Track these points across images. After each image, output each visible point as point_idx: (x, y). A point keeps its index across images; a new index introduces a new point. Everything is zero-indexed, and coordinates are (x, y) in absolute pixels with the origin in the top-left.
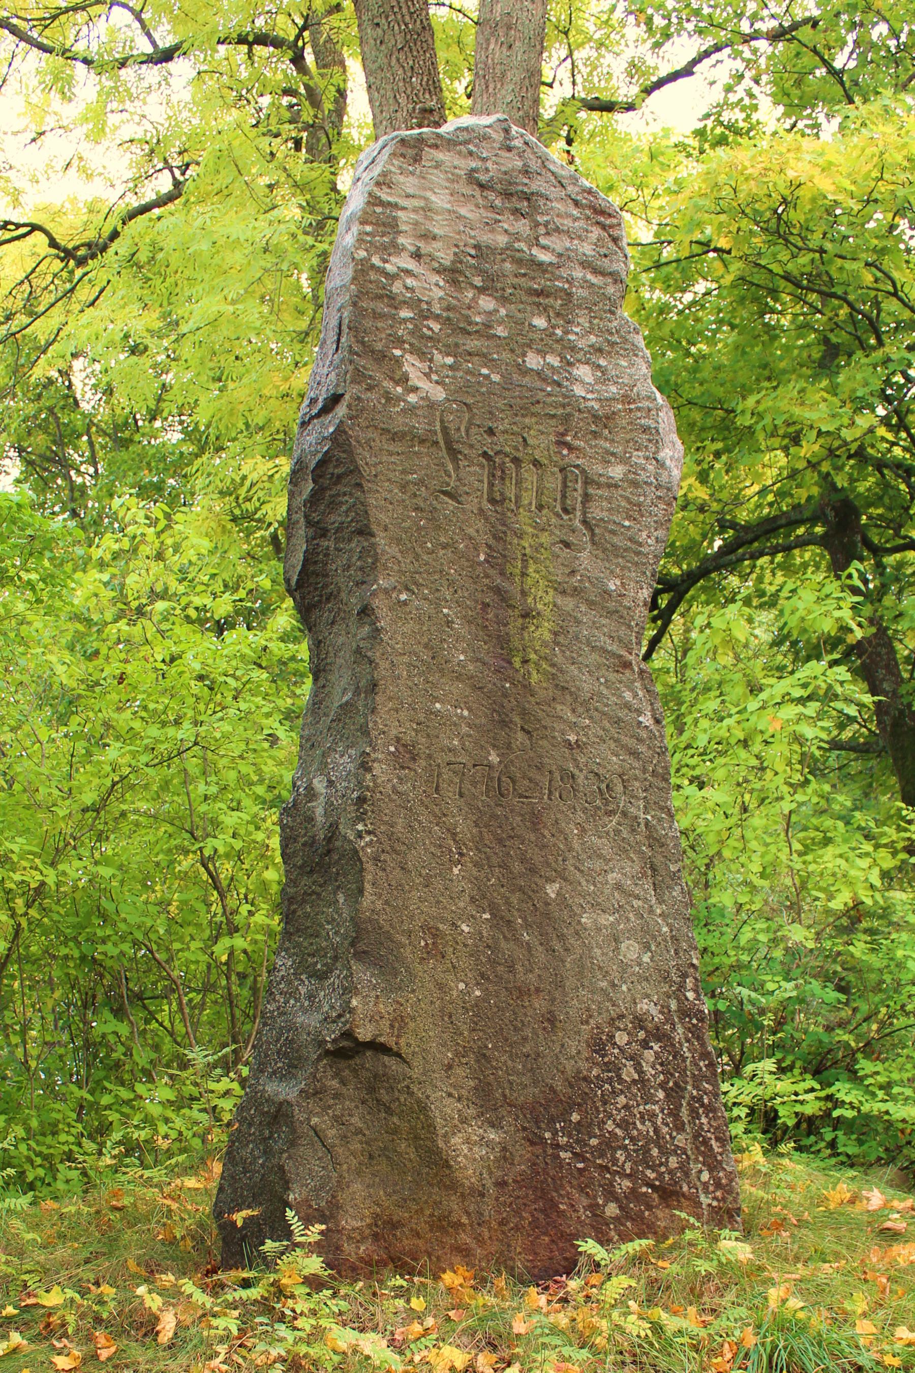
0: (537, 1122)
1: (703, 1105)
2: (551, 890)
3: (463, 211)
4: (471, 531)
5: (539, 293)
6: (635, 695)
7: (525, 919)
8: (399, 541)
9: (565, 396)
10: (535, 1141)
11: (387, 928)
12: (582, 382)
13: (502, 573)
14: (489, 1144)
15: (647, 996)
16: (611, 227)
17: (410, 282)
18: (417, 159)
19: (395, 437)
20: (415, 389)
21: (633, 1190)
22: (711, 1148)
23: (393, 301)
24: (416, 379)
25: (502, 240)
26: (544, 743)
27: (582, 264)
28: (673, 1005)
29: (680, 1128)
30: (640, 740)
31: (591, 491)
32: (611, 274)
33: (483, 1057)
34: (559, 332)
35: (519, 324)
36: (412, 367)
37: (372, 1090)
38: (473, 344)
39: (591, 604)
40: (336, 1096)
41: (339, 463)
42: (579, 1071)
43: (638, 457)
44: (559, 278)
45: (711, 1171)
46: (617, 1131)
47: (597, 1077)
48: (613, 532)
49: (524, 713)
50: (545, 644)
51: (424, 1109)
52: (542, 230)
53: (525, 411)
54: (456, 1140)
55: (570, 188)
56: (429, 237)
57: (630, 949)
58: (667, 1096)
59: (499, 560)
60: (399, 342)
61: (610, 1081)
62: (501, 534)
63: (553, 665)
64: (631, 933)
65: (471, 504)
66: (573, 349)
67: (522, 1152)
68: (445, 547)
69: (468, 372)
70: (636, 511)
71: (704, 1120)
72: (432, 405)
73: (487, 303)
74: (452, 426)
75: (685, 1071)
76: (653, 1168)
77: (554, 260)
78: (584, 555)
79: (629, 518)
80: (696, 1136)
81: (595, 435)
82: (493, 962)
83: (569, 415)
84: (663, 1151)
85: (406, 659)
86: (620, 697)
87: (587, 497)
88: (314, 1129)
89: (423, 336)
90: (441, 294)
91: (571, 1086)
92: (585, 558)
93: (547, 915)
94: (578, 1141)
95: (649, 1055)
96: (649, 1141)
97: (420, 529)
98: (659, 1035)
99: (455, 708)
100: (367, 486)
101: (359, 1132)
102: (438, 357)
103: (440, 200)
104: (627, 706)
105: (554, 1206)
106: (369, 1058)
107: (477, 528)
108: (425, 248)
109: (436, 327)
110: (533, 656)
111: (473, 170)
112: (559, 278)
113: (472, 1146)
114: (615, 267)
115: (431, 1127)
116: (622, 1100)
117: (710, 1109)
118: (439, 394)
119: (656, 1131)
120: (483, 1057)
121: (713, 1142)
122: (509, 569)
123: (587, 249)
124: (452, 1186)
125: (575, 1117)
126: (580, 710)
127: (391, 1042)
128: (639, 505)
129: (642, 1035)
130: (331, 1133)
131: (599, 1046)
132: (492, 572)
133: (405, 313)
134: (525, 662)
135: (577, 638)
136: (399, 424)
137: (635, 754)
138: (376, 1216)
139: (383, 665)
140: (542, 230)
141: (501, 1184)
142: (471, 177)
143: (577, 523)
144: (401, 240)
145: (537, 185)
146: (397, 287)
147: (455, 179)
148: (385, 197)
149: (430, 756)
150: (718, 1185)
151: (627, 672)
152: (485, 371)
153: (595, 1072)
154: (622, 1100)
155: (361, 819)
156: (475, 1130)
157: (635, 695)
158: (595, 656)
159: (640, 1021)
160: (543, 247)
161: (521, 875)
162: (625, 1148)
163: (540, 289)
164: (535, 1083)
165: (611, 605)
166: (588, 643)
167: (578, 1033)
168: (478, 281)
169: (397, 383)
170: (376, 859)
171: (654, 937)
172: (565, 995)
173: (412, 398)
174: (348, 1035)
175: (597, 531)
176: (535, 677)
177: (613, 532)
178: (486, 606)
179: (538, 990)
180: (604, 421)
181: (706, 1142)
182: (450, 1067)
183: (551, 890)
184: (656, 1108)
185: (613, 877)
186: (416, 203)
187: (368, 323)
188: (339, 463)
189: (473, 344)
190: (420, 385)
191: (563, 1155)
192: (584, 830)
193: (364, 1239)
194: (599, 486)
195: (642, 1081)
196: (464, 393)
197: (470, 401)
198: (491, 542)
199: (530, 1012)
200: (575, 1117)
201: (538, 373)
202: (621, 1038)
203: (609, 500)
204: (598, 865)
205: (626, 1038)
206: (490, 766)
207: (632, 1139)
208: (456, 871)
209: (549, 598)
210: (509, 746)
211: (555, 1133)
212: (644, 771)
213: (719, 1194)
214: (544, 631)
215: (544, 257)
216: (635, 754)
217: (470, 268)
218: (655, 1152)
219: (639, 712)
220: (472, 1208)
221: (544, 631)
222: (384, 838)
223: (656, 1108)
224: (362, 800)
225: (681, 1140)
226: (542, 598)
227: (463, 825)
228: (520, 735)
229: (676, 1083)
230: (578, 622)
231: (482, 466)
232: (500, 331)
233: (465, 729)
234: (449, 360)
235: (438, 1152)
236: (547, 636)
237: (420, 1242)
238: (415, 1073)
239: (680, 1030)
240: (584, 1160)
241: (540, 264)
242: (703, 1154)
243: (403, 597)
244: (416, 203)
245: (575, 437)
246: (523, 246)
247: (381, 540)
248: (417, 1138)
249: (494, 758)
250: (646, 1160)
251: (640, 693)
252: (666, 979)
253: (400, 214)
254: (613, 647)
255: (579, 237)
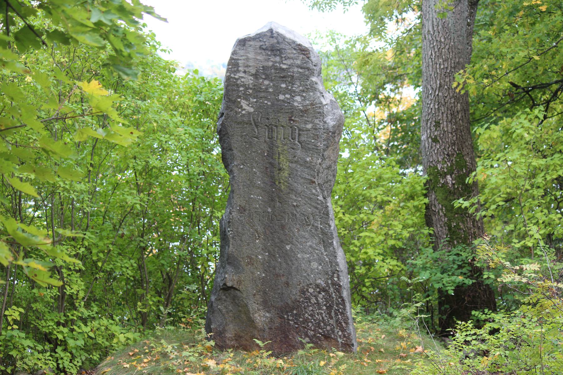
0: (282, 312)
1: (339, 312)
2: (288, 247)
3: (258, 58)
4: (262, 147)
5: (283, 77)
6: (316, 191)
7: (279, 255)
8: (240, 151)
9: (291, 106)
10: (282, 317)
11: (236, 256)
12: (297, 101)
13: (272, 158)
14: (266, 317)
15: (320, 279)
16: (307, 54)
17: (242, 80)
18: (244, 45)
19: (238, 123)
20: (244, 110)
21: (315, 335)
22: (342, 325)
23: (238, 86)
24: (245, 106)
25: (270, 64)
26: (286, 205)
27: (297, 67)
28: (330, 282)
29: (332, 318)
30: (318, 204)
31: (301, 132)
32: (307, 68)
33: (265, 293)
34: (290, 88)
35: (276, 87)
36: (244, 103)
37: (234, 300)
38: (262, 94)
39: (301, 165)
40: (225, 301)
41: (224, 131)
42: (296, 299)
43: (317, 121)
44: (290, 72)
45: (342, 331)
46: (309, 317)
47: (303, 301)
48: (308, 144)
49: (279, 197)
50: (286, 177)
51: (247, 306)
52: (284, 59)
53: (279, 112)
54: (256, 315)
55: (292, 45)
56: (248, 66)
57: (314, 265)
58: (327, 308)
59: (271, 155)
60: (240, 97)
61: (307, 302)
62: (272, 146)
63: (289, 183)
64: (315, 260)
65: (262, 140)
66: (294, 92)
67: (277, 321)
68: (254, 152)
69: (261, 103)
70: (316, 137)
71: (340, 316)
72: (249, 113)
73: (266, 82)
74: (256, 119)
75: (333, 301)
76: (321, 329)
77: (288, 67)
78: (299, 152)
79: (314, 139)
80: (337, 321)
81: (302, 116)
82: (269, 267)
83: (293, 111)
84: (325, 324)
85: (242, 184)
86: (311, 191)
87: (299, 135)
88: (219, 309)
89: (247, 94)
90: (252, 82)
91: (294, 303)
92: (299, 152)
93: (287, 254)
94: (296, 319)
95: (321, 296)
96: (320, 321)
97: (246, 148)
98: (324, 290)
99: (257, 197)
100: (230, 137)
101: (231, 311)
102: (251, 100)
103: (251, 55)
104: (314, 194)
105: (288, 337)
106: (232, 291)
107: (264, 146)
108: (247, 70)
109: (251, 91)
110: (282, 181)
111: (262, 45)
112: (290, 72)
113: (261, 317)
114: (308, 66)
115: (248, 311)
116: (311, 308)
117: (342, 313)
118: (252, 110)
119: (323, 318)
120: (265, 293)
121: (343, 323)
122: (274, 157)
123: (298, 62)
124: (255, 328)
125: (295, 312)
126: (298, 196)
127: (237, 287)
128: (317, 135)
129: (318, 290)
130: (224, 310)
131: (303, 292)
132: (269, 158)
133: (241, 89)
134: (280, 183)
135: (296, 175)
136: (240, 120)
137: (317, 208)
138: (236, 334)
139: (236, 185)
140: (284, 59)
141: (270, 329)
142: (261, 48)
143: (296, 142)
144: (240, 69)
145: (282, 46)
146: (239, 82)
147: (256, 49)
148: (235, 57)
149: (250, 210)
150: (344, 336)
151: (314, 184)
152: (266, 102)
153: (301, 300)
154: (311, 308)
155: (229, 227)
156: (262, 313)
157: (316, 191)
158: (302, 180)
159: (317, 286)
160: (284, 64)
161: (278, 243)
162: (312, 322)
163: (284, 76)
164: (282, 301)
165: (308, 165)
166: (300, 177)
167: (296, 288)
168: (263, 77)
169: (239, 108)
170: (233, 238)
171: (323, 262)
172: (292, 277)
173: (244, 112)
174: (225, 284)
175: (303, 144)
176: (283, 187)
177: (308, 144)
178: (267, 168)
179: (283, 275)
180: (305, 111)
181: (340, 323)
182: (254, 295)
183: (288, 247)
184: (323, 312)
185: (308, 244)
186: (244, 58)
187: (230, 93)
188: (224, 131)
189: (262, 94)
190: (246, 108)
191: (290, 322)
192: (299, 230)
193: (232, 340)
194: (303, 131)
195: (318, 303)
196: (259, 108)
197: (261, 111)
198: (269, 150)
199: (280, 281)
200: (295, 312)
201: (283, 100)
202: (311, 290)
203: (307, 135)
204: (304, 240)
205: (313, 290)
206: (268, 212)
207: (314, 320)
208: (257, 241)
209: (287, 164)
210: (274, 207)
211: (288, 316)
212: (320, 213)
213: (345, 339)
214: (286, 174)
215: (284, 67)
216: (317, 208)
217: (262, 73)
218: (322, 324)
219: (318, 196)
220: (261, 334)
221: (286, 174)
222: (235, 232)
223: (323, 312)
224: (229, 222)
225: (331, 322)
226: (285, 165)
227: (260, 229)
228: (278, 203)
229: (330, 305)
230: (297, 171)
231: (265, 129)
232: (271, 90)
233: (260, 202)
234: (255, 100)
235: (251, 318)
236: (287, 175)
237: (248, 343)
238: (244, 296)
239: (332, 289)
240: (298, 324)
241: (283, 69)
242: (339, 326)
243: (242, 167)
244: (244, 58)
245: (295, 117)
246: (278, 64)
247: (235, 151)
248: (246, 314)
249: (269, 210)
250: (319, 327)
251: (318, 190)
252: (327, 274)
253: (239, 61)
254: (309, 177)
255: (296, 59)
